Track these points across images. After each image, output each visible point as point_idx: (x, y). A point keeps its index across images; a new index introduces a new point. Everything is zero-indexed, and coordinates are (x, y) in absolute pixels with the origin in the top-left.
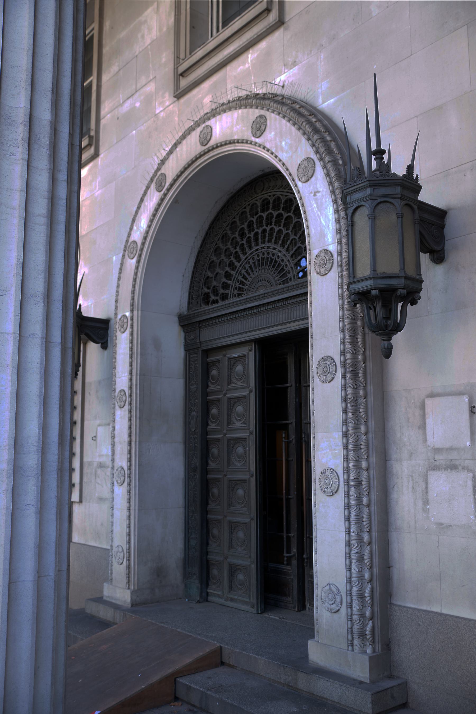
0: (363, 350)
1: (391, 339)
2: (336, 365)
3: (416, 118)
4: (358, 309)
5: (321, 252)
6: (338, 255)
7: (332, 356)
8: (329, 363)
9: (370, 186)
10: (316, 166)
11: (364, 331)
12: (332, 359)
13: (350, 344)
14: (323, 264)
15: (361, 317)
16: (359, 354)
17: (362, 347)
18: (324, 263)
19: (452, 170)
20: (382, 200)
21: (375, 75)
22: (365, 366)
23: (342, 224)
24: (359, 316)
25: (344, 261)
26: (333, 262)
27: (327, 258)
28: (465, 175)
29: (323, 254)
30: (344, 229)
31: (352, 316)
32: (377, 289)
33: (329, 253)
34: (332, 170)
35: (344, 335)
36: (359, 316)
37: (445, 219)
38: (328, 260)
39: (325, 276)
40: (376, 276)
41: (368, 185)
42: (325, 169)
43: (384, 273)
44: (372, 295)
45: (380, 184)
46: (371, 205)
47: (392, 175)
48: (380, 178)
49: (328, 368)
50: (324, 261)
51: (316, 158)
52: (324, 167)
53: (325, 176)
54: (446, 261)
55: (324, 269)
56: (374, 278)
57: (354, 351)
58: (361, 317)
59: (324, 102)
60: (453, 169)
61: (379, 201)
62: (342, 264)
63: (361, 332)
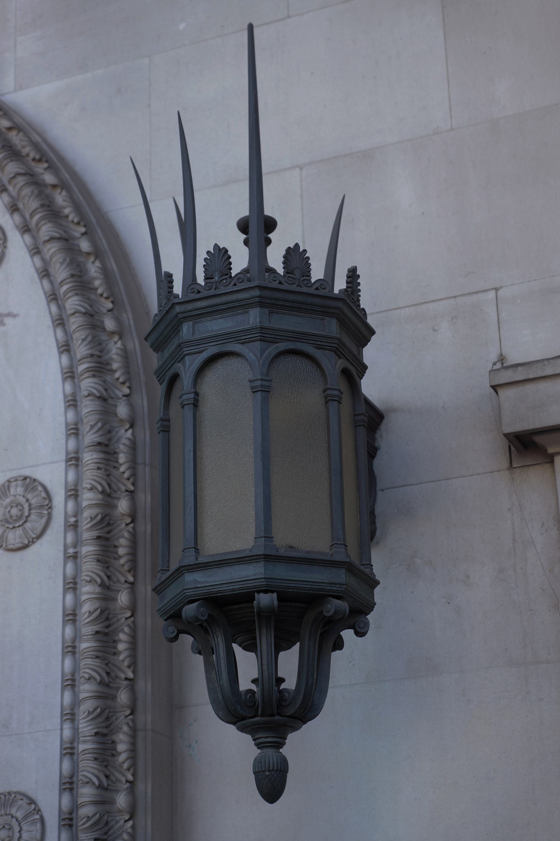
0: (130, 778)
1: (284, 744)
2: (42, 820)
3: (298, 170)
4: (122, 657)
5: (13, 484)
6: (67, 497)
7: (31, 793)
8: (19, 815)
9: (262, 303)
10: (9, 244)
11: (133, 721)
12: (32, 801)
13: (96, 759)
14: (19, 518)
15: (126, 679)
16: (117, 791)
17: (128, 769)
18: (22, 515)
19: (398, 311)
20: (291, 345)
21: (251, 28)
22: (133, 827)
23: (85, 411)
24: (123, 676)
25: (87, 514)
26: (50, 516)
27: (33, 501)
28: (434, 330)
29: (20, 490)
30: (92, 427)
31: (104, 674)
32: (273, 592)
33: (40, 488)
34: (61, 263)
35: (75, 730)
36: (123, 676)
37: (377, 435)
38: (35, 508)
39: (19, 554)
40: (274, 553)
41: (257, 300)
42: (39, 256)
43: (291, 547)
44: (259, 608)
45: (286, 304)
46: (261, 355)
47: (318, 285)
48: (285, 286)
49: (17, 829)
50: (22, 510)
51: (10, 222)
52: (35, 251)
53: (36, 276)
54: (377, 543)
55: (19, 531)
56: (268, 558)
57: (104, 780)
58: (126, 679)
59: (20, 87)
60: (403, 310)
61: (283, 346)
62: (76, 521)
63: (128, 724)
